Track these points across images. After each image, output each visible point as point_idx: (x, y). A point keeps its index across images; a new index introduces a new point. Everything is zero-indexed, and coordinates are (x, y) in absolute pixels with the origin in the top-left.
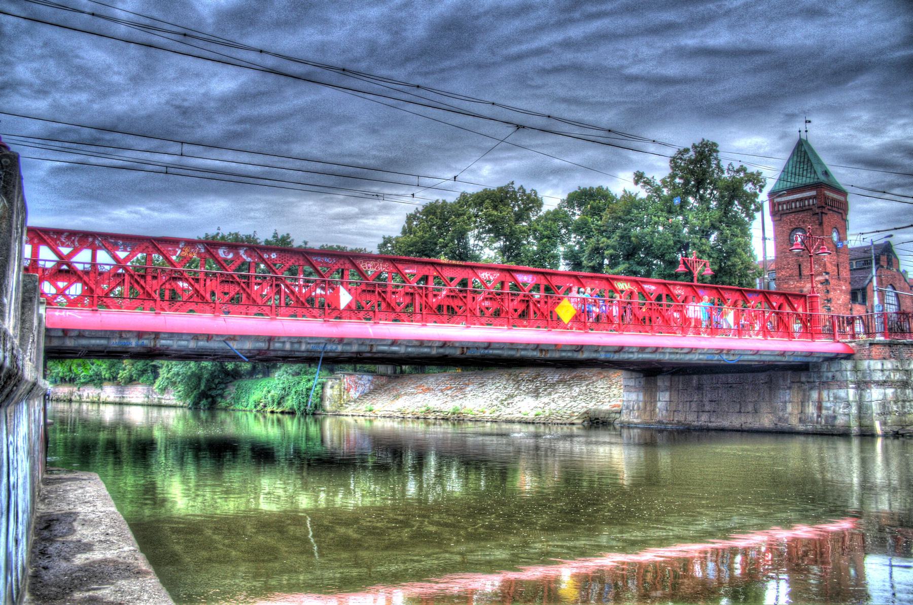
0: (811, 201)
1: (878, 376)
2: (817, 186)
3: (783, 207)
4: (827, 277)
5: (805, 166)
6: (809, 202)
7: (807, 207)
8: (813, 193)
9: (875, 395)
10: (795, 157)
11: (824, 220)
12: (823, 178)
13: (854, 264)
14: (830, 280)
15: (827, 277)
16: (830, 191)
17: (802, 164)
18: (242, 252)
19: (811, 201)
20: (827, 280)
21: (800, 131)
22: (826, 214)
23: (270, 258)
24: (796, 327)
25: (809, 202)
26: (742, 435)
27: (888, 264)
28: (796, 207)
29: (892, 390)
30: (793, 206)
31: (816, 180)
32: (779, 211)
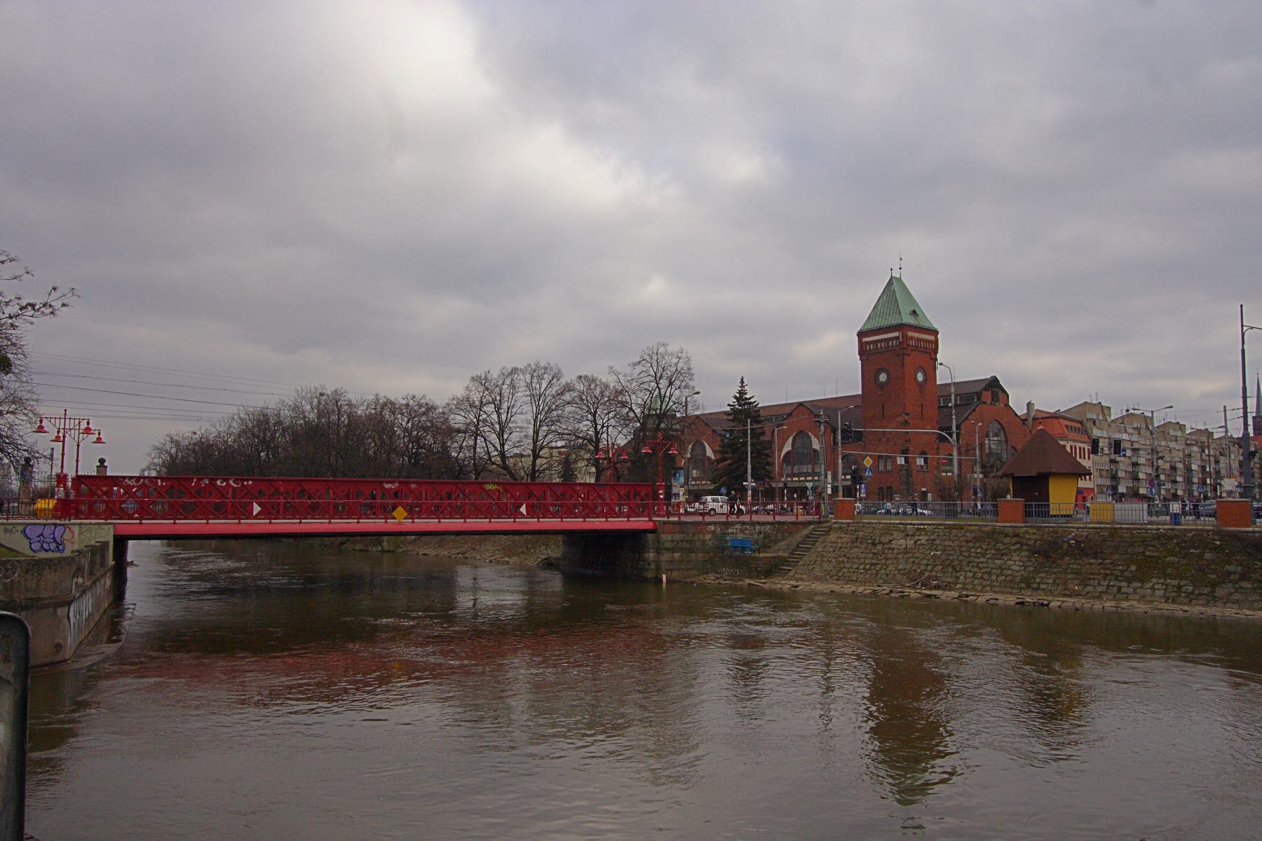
1: (669, 545)
2: (900, 327)
3: (870, 347)
7: (891, 348)
8: (896, 334)
9: (666, 557)
10: (885, 296)
11: (905, 361)
12: (908, 320)
14: (910, 421)
17: (890, 304)
18: (231, 482)
19: (894, 342)
21: (892, 270)
22: (909, 355)
23: (248, 484)
27: (993, 399)
28: (881, 347)
29: (679, 554)
32: (866, 350)
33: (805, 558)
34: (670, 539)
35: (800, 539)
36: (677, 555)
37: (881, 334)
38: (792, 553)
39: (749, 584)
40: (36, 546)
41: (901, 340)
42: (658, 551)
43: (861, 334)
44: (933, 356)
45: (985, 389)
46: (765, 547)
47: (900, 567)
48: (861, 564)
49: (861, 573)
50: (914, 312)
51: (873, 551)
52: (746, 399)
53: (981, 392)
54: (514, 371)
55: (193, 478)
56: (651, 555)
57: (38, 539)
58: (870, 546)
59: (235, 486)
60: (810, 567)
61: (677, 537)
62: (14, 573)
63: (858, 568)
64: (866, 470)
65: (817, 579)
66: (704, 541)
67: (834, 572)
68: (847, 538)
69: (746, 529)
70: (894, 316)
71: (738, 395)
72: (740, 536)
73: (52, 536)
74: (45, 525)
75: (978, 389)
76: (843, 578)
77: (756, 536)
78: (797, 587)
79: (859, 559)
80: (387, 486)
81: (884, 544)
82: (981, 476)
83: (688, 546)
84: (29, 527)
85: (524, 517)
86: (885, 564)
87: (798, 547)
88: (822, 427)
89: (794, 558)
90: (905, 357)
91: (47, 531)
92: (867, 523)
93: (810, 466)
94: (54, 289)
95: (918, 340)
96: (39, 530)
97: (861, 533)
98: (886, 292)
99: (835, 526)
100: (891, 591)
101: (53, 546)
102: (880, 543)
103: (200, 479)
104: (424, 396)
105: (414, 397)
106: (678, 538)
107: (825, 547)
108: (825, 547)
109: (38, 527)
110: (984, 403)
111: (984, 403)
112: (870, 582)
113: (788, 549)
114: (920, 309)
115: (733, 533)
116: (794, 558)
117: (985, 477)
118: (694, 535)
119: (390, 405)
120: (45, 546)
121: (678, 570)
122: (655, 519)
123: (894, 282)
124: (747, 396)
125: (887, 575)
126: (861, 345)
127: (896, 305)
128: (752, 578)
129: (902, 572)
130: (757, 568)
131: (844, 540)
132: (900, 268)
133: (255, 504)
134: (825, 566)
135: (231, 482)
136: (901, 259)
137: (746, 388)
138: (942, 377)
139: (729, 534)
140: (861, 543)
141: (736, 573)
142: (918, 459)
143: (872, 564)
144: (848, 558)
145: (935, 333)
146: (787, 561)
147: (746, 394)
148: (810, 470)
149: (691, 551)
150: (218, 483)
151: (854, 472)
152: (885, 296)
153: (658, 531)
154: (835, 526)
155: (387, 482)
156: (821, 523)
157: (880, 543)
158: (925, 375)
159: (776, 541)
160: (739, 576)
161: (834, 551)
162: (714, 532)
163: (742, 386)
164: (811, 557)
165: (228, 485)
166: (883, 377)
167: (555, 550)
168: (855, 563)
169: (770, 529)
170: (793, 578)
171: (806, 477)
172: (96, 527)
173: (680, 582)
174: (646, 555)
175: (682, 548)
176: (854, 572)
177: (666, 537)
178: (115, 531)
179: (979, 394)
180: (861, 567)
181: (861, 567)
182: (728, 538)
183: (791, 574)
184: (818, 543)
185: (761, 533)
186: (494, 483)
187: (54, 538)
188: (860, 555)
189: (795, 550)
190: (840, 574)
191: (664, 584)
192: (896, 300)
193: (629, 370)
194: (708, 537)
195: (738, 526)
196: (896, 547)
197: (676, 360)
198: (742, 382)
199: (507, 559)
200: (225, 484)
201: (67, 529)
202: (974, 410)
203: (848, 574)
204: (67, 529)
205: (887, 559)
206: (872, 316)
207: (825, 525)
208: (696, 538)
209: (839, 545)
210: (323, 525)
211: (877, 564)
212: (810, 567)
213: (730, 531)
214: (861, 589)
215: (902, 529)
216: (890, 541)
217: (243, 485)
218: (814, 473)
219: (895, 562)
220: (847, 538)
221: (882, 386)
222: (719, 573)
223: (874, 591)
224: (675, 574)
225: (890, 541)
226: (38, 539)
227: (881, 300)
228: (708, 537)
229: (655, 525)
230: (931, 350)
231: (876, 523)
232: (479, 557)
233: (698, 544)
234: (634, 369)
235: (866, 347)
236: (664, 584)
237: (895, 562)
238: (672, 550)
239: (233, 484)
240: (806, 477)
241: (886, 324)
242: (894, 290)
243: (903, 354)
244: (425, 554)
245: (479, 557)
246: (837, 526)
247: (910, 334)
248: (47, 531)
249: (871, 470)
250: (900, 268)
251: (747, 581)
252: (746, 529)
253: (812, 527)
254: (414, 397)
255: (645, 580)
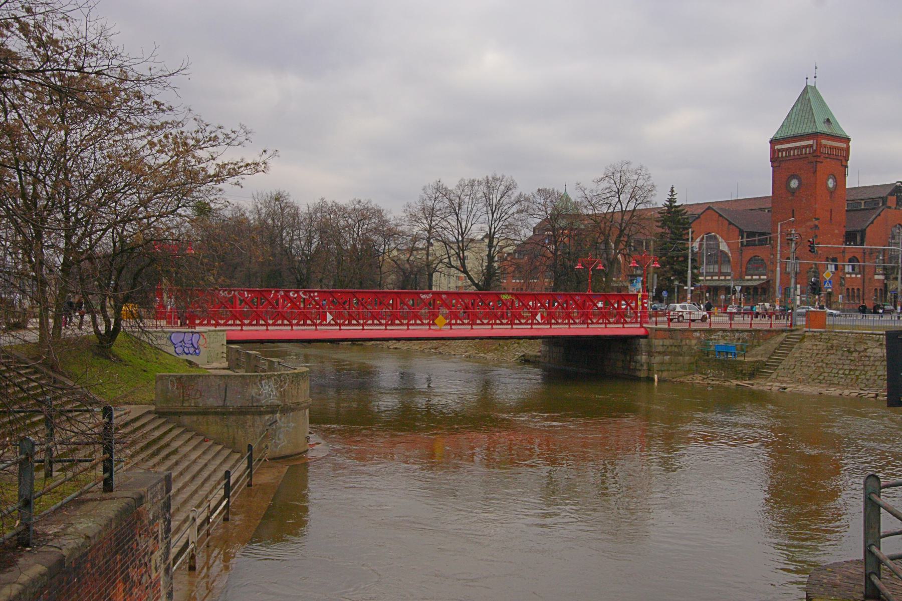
0: (808, 149)
1: (660, 349)
2: (815, 135)
3: (782, 154)
4: (817, 222)
5: (807, 115)
6: (806, 151)
7: (804, 156)
8: (810, 142)
9: (657, 359)
10: (799, 105)
11: (818, 168)
12: (822, 128)
13: (863, 204)
14: (819, 226)
15: (817, 222)
16: (825, 139)
19: (808, 149)
20: (816, 226)
24: (575, 312)
25: (806, 151)
26: (431, 460)
28: (794, 155)
30: (780, 155)
31: (814, 130)
32: (778, 157)
33: (783, 362)
34: (661, 344)
35: (776, 346)
36: (667, 358)
37: (795, 142)
38: (770, 358)
39: (737, 385)
40: (179, 350)
41: (815, 148)
42: (650, 354)
43: (773, 142)
44: (844, 164)
45: (891, 194)
46: (744, 351)
47: (879, 373)
48: (839, 369)
49: (842, 378)
50: (828, 120)
51: (849, 358)
52: (676, 207)
53: (887, 197)
54: (472, 183)
55: (271, 291)
56: (643, 358)
57: (180, 344)
58: (846, 354)
59: (304, 297)
60: (791, 371)
61: (668, 342)
62: (285, 383)
63: (838, 373)
64: (825, 282)
65: (799, 381)
66: (690, 346)
67: (815, 376)
68: (822, 345)
69: (727, 336)
70: (808, 124)
71: (668, 203)
72: (722, 342)
73: (190, 342)
74: (185, 333)
75: (884, 194)
76: (824, 381)
77: (735, 342)
78: (785, 389)
79: (837, 365)
80: (423, 297)
81: (860, 352)
82: (882, 277)
83: (676, 350)
84: (173, 334)
85: (539, 324)
86: (864, 370)
87: (775, 352)
88: (793, 245)
89: (773, 362)
90: (818, 164)
91: (187, 338)
92: (839, 332)
93: (717, 266)
94: (265, 151)
95: (831, 148)
96: (181, 336)
97: (835, 342)
98: (800, 101)
99: (807, 334)
100: (877, 395)
101: (191, 350)
102: (856, 351)
103: (277, 292)
104: (369, 201)
105: (360, 201)
106: (668, 343)
107: (801, 353)
108: (801, 353)
109: (179, 334)
110: (890, 207)
111: (890, 207)
112: (851, 386)
113: (765, 353)
114: (833, 117)
115: (715, 339)
116: (773, 362)
117: (886, 278)
118: (681, 341)
119: (336, 210)
120: (186, 350)
121: (668, 370)
122: (645, 325)
123: (809, 90)
124: (676, 204)
125: (868, 380)
126: (773, 151)
127: (811, 113)
128: (737, 379)
129: (881, 377)
130: (742, 371)
131: (819, 347)
132: (815, 77)
133: (328, 313)
134: (805, 370)
135: (301, 293)
136: (816, 68)
137: (675, 197)
138: (851, 182)
139: (711, 340)
140: (837, 350)
141: (722, 374)
142: (846, 267)
143: (851, 370)
144: (827, 364)
145: (847, 140)
146: (766, 365)
147: (675, 202)
148: (717, 270)
149: (679, 354)
150: (291, 294)
151: (814, 284)
152: (799, 105)
153: (650, 337)
154: (807, 334)
155: (423, 293)
156: (792, 331)
157: (856, 351)
158: (836, 181)
159: (753, 347)
160: (724, 377)
161: (811, 357)
162: (699, 338)
163: (672, 195)
164: (788, 362)
165: (299, 296)
166: (794, 184)
167: (535, 350)
168: (833, 368)
169: (747, 336)
170: (776, 380)
171: (712, 276)
172: (214, 333)
173: (670, 381)
174: (639, 357)
175: (671, 352)
176: (835, 376)
177: (658, 343)
178: (227, 337)
179: (884, 200)
180: (841, 372)
181: (841, 372)
182: (711, 344)
183: (774, 376)
184: (793, 350)
185: (739, 339)
186: (509, 294)
187: (192, 344)
188: (838, 362)
189: (772, 355)
190: (821, 378)
191: (656, 384)
192: (811, 109)
193: (593, 186)
194: (694, 342)
195: (720, 333)
196: (872, 355)
197: (636, 177)
198: (672, 191)
199: (482, 355)
200: (296, 295)
201: (201, 337)
202: (879, 215)
203: (829, 378)
204: (201, 337)
205: (864, 366)
206: (785, 124)
207: (796, 333)
208: (684, 343)
209: (815, 351)
210: (394, 331)
211: (857, 370)
212: (791, 371)
213: (713, 337)
214: (846, 392)
215: (877, 339)
216: (866, 349)
217: (310, 296)
218: (721, 273)
219: (873, 368)
220: (822, 345)
221: (793, 192)
222: (705, 374)
223: (860, 394)
224: (665, 374)
225: (866, 349)
226: (180, 344)
227: (795, 108)
228: (694, 342)
229: (647, 331)
230: (842, 157)
231: (849, 333)
232: (453, 353)
233: (685, 349)
234: (598, 185)
235: (778, 155)
236: (656, 384)
237: (873, 368)
238: (664, 353)
239: (302, 296)
240: (712, 276)
241: (807, 131)
242: (809, 99)
243: (816, 162)
244: (396, 348)
245: (453, 353)
246: (810, 334)
247: (824, 142)
248: (187, 338)
249: (830, 282)
250: (815, 77)
251: (735, 382)
252: (727, 336)
253: (785, 334)
254: (360, 201)
255: (638, 379)
